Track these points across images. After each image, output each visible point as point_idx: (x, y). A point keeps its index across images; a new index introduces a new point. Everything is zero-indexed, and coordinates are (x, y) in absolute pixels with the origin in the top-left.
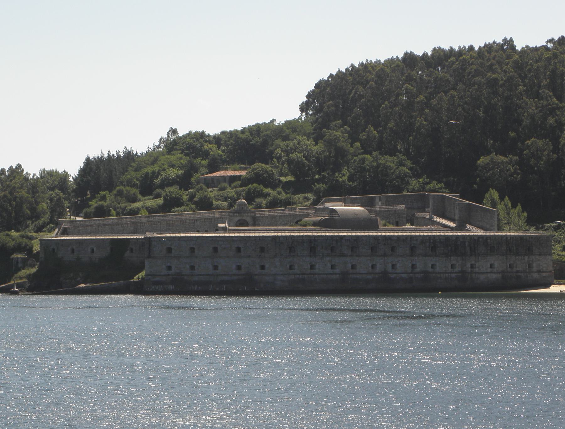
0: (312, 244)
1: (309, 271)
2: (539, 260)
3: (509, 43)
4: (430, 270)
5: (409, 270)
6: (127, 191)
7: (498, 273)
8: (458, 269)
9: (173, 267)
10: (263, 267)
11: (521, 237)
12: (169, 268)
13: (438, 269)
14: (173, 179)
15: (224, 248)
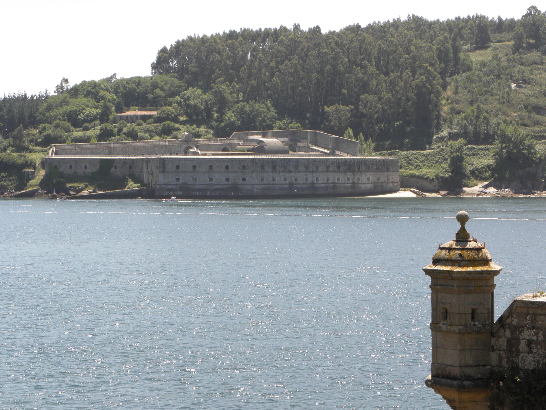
0: (243, 164)
1: (272, 182)
3: (438, 20)
4: (337, 181)
5: (325, 182)
6: (62, 124)
7: (371, 183)
8: (351, 181)
9: (181, 179)
10: (244, 180)
11: (384, 160)
12: (178, 179)
13: (340, 181)
14: (94, 116)
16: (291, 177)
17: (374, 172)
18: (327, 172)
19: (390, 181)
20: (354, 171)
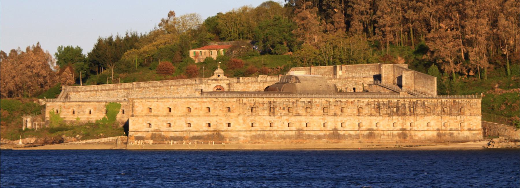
1: (269, 128)
2: (470, 120)
4: (375, 128)
5: (357, 128)
7: (433, 130)
10: (229, 125)
13: (381, 128)
15: (196, 109)
16: (301, 122)
17: (438, 115)
18: (359, 116)
19: (466, 128)
20: (404, 114)
